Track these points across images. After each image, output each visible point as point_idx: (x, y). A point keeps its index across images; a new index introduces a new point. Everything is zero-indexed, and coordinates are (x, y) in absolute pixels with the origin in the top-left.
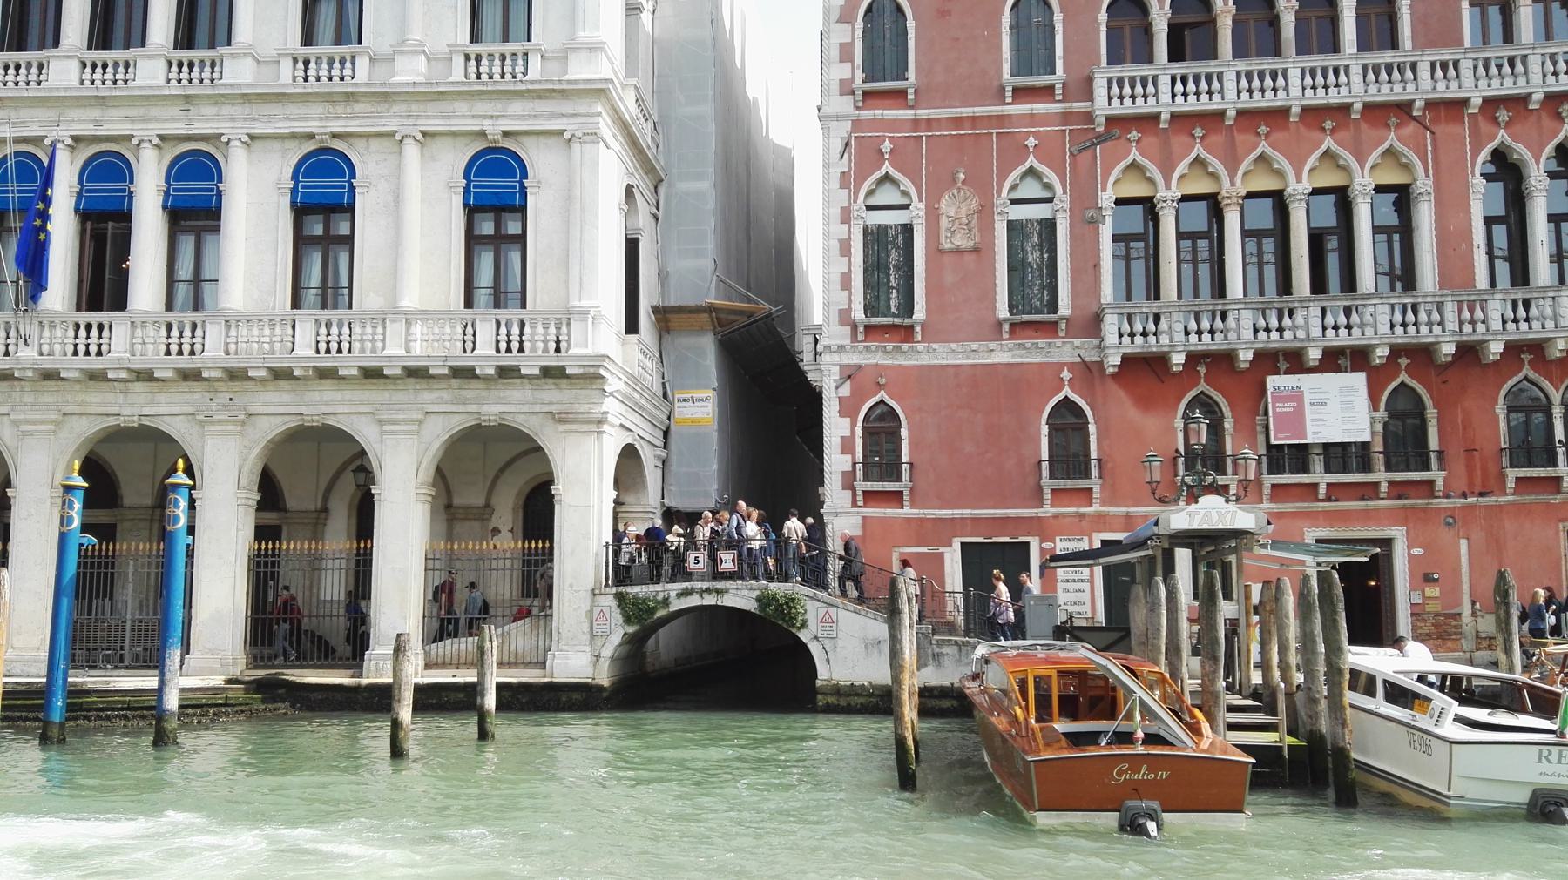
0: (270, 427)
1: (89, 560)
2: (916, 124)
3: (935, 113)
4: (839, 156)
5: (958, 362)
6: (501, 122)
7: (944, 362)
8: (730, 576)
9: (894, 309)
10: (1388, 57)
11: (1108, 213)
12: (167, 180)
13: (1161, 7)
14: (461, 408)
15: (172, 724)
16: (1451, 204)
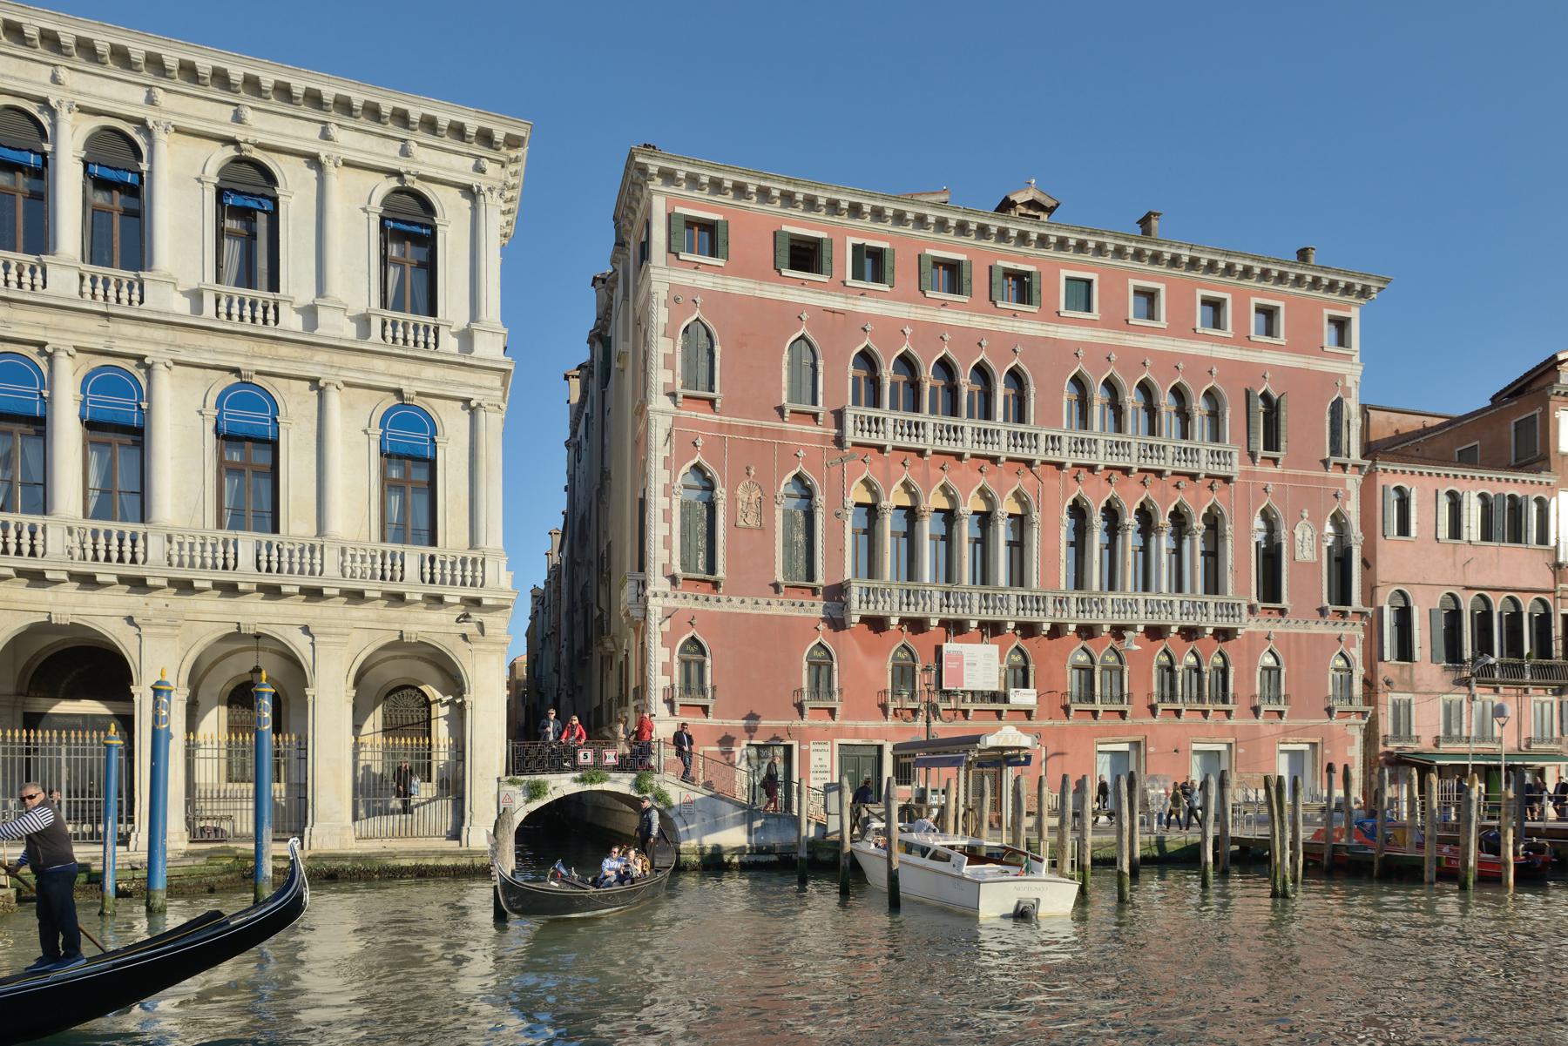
0: (208, 634)
1: (80, 747)
2: (720, 426)
3: (735, 421)
4: (663, 443)
5: (748, 612)
6: (416, 383)
7: (738, 611)
10: (1021, 428)
11: (850, 513)
12: (83, 391)
13: (888, 368)
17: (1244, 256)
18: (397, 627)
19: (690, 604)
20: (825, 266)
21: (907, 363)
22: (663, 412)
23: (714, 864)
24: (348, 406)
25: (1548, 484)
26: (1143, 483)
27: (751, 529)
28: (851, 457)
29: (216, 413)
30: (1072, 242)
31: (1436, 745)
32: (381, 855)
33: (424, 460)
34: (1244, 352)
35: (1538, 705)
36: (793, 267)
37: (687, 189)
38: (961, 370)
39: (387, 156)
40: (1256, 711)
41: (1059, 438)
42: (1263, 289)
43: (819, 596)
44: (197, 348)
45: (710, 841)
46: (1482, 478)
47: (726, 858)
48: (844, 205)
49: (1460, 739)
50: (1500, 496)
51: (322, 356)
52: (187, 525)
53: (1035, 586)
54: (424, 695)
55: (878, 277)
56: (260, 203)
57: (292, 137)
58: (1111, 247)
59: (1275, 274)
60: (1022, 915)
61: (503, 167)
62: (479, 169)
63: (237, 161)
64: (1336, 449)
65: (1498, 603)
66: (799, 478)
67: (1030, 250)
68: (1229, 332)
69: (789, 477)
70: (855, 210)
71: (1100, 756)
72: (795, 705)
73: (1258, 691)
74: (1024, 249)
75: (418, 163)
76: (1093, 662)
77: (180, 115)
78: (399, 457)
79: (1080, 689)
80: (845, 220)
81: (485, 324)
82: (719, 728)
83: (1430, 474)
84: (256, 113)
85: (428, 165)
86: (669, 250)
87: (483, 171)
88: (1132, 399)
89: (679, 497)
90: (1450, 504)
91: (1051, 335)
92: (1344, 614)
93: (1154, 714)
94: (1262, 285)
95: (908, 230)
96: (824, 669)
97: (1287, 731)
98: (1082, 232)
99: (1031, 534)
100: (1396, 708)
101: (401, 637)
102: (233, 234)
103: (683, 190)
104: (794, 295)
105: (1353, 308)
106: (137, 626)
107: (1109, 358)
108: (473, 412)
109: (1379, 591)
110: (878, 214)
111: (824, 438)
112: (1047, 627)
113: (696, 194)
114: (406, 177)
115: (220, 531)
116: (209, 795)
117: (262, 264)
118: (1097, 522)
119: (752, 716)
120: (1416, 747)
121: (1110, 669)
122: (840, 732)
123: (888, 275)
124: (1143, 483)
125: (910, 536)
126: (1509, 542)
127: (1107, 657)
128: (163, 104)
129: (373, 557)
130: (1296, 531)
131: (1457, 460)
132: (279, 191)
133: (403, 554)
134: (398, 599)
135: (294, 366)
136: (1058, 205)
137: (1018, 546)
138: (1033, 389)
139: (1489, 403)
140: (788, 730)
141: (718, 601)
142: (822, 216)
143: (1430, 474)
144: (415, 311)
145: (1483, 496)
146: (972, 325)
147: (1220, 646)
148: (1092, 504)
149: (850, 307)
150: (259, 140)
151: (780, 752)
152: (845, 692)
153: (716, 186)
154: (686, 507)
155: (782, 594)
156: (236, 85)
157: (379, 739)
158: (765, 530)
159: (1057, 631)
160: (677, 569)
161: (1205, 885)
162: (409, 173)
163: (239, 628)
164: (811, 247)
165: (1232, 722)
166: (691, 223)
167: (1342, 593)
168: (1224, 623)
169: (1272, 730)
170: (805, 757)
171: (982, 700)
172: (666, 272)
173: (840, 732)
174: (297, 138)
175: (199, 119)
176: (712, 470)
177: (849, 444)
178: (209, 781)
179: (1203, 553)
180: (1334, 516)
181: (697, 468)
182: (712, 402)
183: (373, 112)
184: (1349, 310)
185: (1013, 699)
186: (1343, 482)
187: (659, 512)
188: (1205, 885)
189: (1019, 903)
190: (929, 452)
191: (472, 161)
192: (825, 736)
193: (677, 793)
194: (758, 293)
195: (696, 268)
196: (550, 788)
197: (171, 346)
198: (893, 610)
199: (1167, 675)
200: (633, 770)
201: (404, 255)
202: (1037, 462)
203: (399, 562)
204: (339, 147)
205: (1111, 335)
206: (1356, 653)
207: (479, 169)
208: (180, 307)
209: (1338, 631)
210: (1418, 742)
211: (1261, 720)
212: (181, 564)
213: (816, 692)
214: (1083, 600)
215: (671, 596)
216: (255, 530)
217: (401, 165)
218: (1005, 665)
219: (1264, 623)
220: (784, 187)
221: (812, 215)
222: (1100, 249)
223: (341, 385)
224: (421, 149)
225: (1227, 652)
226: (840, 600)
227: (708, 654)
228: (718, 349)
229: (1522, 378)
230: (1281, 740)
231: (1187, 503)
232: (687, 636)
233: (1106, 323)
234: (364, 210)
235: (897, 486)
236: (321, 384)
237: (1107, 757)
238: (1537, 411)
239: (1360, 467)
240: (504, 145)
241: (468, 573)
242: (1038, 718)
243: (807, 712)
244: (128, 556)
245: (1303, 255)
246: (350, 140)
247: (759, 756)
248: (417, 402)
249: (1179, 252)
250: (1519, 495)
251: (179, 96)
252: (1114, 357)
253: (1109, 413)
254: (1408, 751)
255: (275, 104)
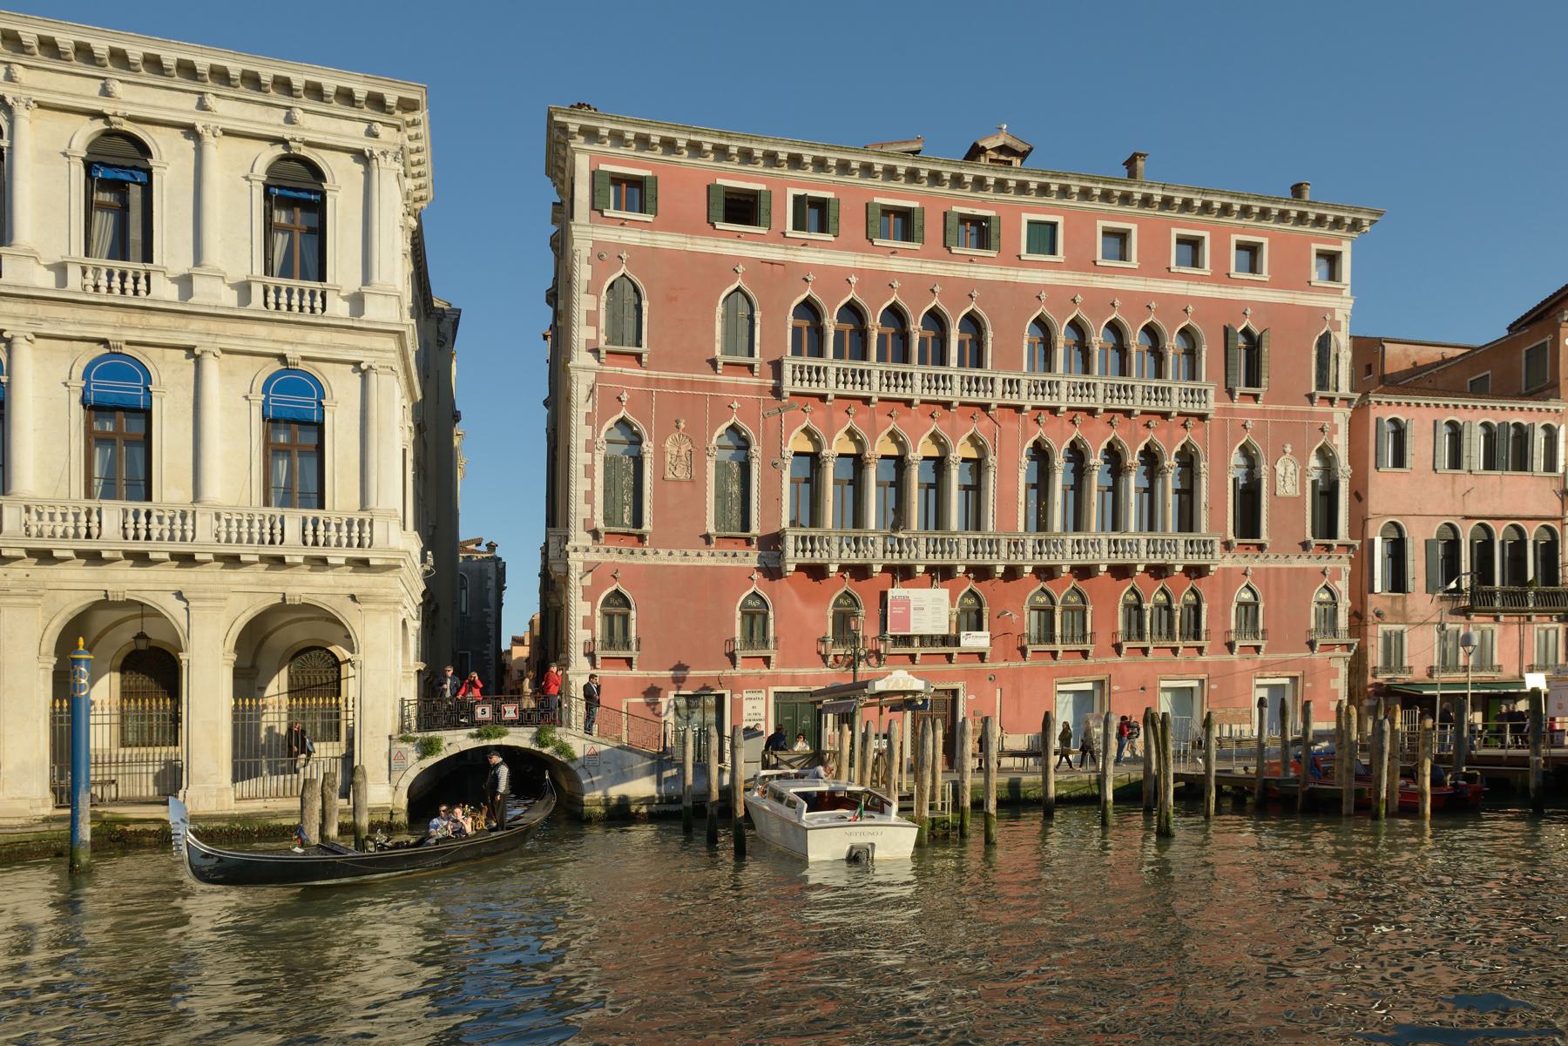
0: (73, 603)
2: (648, 380)
6: (300, 348)
7: (666, 563)
8: (512, 723)
9: (626, 521)
10: (977, 373)
11: (788, 463)
14: (266, 589)
15: (84, 858)
16: (1008, 474)
17: (1222, 194)
18: (279, 589)
19: (614, 558)
20: (763, 218)
21: (935, 319)
22: (585, 369)
23: (620, 815)
24: (229, 373)
25: (1557, 411)
26: (1110, 423)
27: (679, 481)
28: (790, 407)
29: (83, 384)
30: (1033, 186)
31: (1430, 675)
32: (260, 815)
33: (309, 423)
34: (1223, 290)
35: (1542, 632)
36: (728, 219)
37: (612, 146)
38: (911, 317)
39: (270, 124)
40: (1230, 646)
41: (1018, 381)
42: (1244, 226)
43: (754, 546)
44: (59, 321)
45: (615, 792)
46: (1484, 408)
47: (633, 809)
48: (783, 157)
49: (1456, 668)
50: (1504, 425)
51: (197, 324)
52: (51, 495)
53: (990, 528)
54: (333, 655)
55: (907, 235)
56: (132, 175)
57: (166, 108)
58: (1075, 189)
59: (1256, 210)
60: (857, 858)
61: (399, 130)
62: (372, 134)
63: (109, 134)
64: (1323, 383)
65: (1500, 531)
66: (734, 429)
67: (989, 195)
68: (1207, 270)
69: (722, 429)
70: (795, 161)
71: (1060, 697)
72: (726, 655)
73: (1233, 626)
74: (981, 195)
75: (304, 129)
76: (1053, 602)
77: (42, 90)
78: (289, 422)
79: (1039, 630)
80: (785, 171)
81: (376, 287)
82: (644, 680)
83: (1428, 405)
84: (126, 85)
85: (315, 131)
86: (593, 208)
87: (376, 136)
88: (1098, 339)
89: (603, 452)
90: (1450, 435)
91: (1011, 279)
92: (1329, 548)
93: (1119, 652)
94: (1244, 221)
95: (855, 179)
96: (759, 619)
97: (1264, 666)
98: (1043, 175)
99: (988, 478)
100: (1387, 638)
101: (284, 599)
102: (103, 207)
103: (608, 147)
104: (728, 248)
105: (1344, 242)
106: (186, 600)
107: (1074, 300)
108: (364, 375)
109: (1371, 524)
110: (820, 164)
111: (760, 389)
112: (1000, 569)
113: (622, 150)
114: (291, 143)
115: (267, 509)
116: (107, 760)
117: (135, 234)
118: (1060, 462)
119: (681, 667)
120: (1408, 678)
121: (1073, 610)
122: (775, 680)
123: (832, 226)
124: (1110, 423)
125: (857, 484)
126: (1513, 470)
127: (1069, 598)
128: (23, 81)
129: (76, 516)
130: (1278, 467)
131: (1468, 390)
132: (151, 162)
133: (282, 518)
134: (278, 562)
135: (167, 335)
136: (1031, 149)
137: (974, 490)
138: (990, 334)
139: (1506, 333)
140: (720, 681)
141: (644, 554)
142: (760, 168)
143: (1428, 405)
144: (304, 277)
145: (1486, 425)
146: (924, 271)
147: (1192, 583)
148: (1054, 446)
149: (790, 258)
150: (129, 113)
151: (711, 701)
152: (781, 641)
153: (643, 142)
154: (610, 463)
155: (713, 546)
156: (135, 64)
157: (285, 699)
158: (696, 482)
159: (1012, 573)
160: (599, 524)
161: (1104, 824)
162: (294, 140)
163: (106, 596)
164: (751, 200)
165: (1204, 658)
166: (617, 180)
167: (1327, 526)
168: (1194, 560)
169: (1248, 665)
170: (737, 706)
171: (932, 645)
172: (590, 229)
173: (775, 680)
174: (171, 109)
175: (64, 94)
176: (639, 425)
177: (786, 394)
178: (99, 746)
179: (1177, 491)
180: (1318, 451)
181: (734, 429)
182: (638, 357)
183: (252, 80)
184: (1340, 244)
185: (963, 642)
186: (1330, 416)
187: (581, 469)
188: (1104, 824)
189: (852, 848)
190: (875, 400)
191: (365, 126)
192: (759, 684)
193: (579, 745)
194: (689, 248)
195: (622, 224)
196: (444, 744)
197: (32, 320)
198: (835, 556)
199: (1134, 613)
200: (536, 724)
201: (293, 221)
202: (993, 406)
203: (278, 526)
204: (218, 116)
205: (1077, 277)
206: (1342, 586)
207: (372, 134)
208: (45, 281)
209: (1322, 564)
210: (1410, 672)
211: (1236, 656)
212: (228, 540)
213: (749, 641)
214: (1192, 542)
215: (592, 550)
216: (301, 506)
217: (286, 132)
218: (957, 609)
219: (1241, 559)
220: (717, 141)
221: (749, 168)
222: (1064, 192)
223: (219, 353)
224: (222, 102)
225: (1201, 590)
226: (776, 549)
227: (771, 608)
228: (645, 304)
229: (1539, 306)
230: (1258, 674)
231: (1158, 441)
232: (609, 590)
233: (1072, 265)
234: (247, 178)
235: (841, 434)
236: (197, 352)
237: (1070, 697)
238: (1548, 339)
239: (1349, 401)
240: (398, 109)
241: (355, 534)
242: (992, 660)
243: (739, 661)
244: (178, 534)
245: (1297, 191)
246: (228, 110)
247: (688, 706)
248: (302, 366)
249: (1150, 191)
250: (1525, 423)
251: (42, 72)
252: (1079, 299)
253: (1076, 354)
254: (1399, 681)
255: (145, 76)
